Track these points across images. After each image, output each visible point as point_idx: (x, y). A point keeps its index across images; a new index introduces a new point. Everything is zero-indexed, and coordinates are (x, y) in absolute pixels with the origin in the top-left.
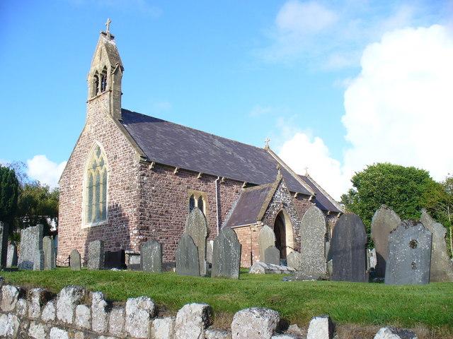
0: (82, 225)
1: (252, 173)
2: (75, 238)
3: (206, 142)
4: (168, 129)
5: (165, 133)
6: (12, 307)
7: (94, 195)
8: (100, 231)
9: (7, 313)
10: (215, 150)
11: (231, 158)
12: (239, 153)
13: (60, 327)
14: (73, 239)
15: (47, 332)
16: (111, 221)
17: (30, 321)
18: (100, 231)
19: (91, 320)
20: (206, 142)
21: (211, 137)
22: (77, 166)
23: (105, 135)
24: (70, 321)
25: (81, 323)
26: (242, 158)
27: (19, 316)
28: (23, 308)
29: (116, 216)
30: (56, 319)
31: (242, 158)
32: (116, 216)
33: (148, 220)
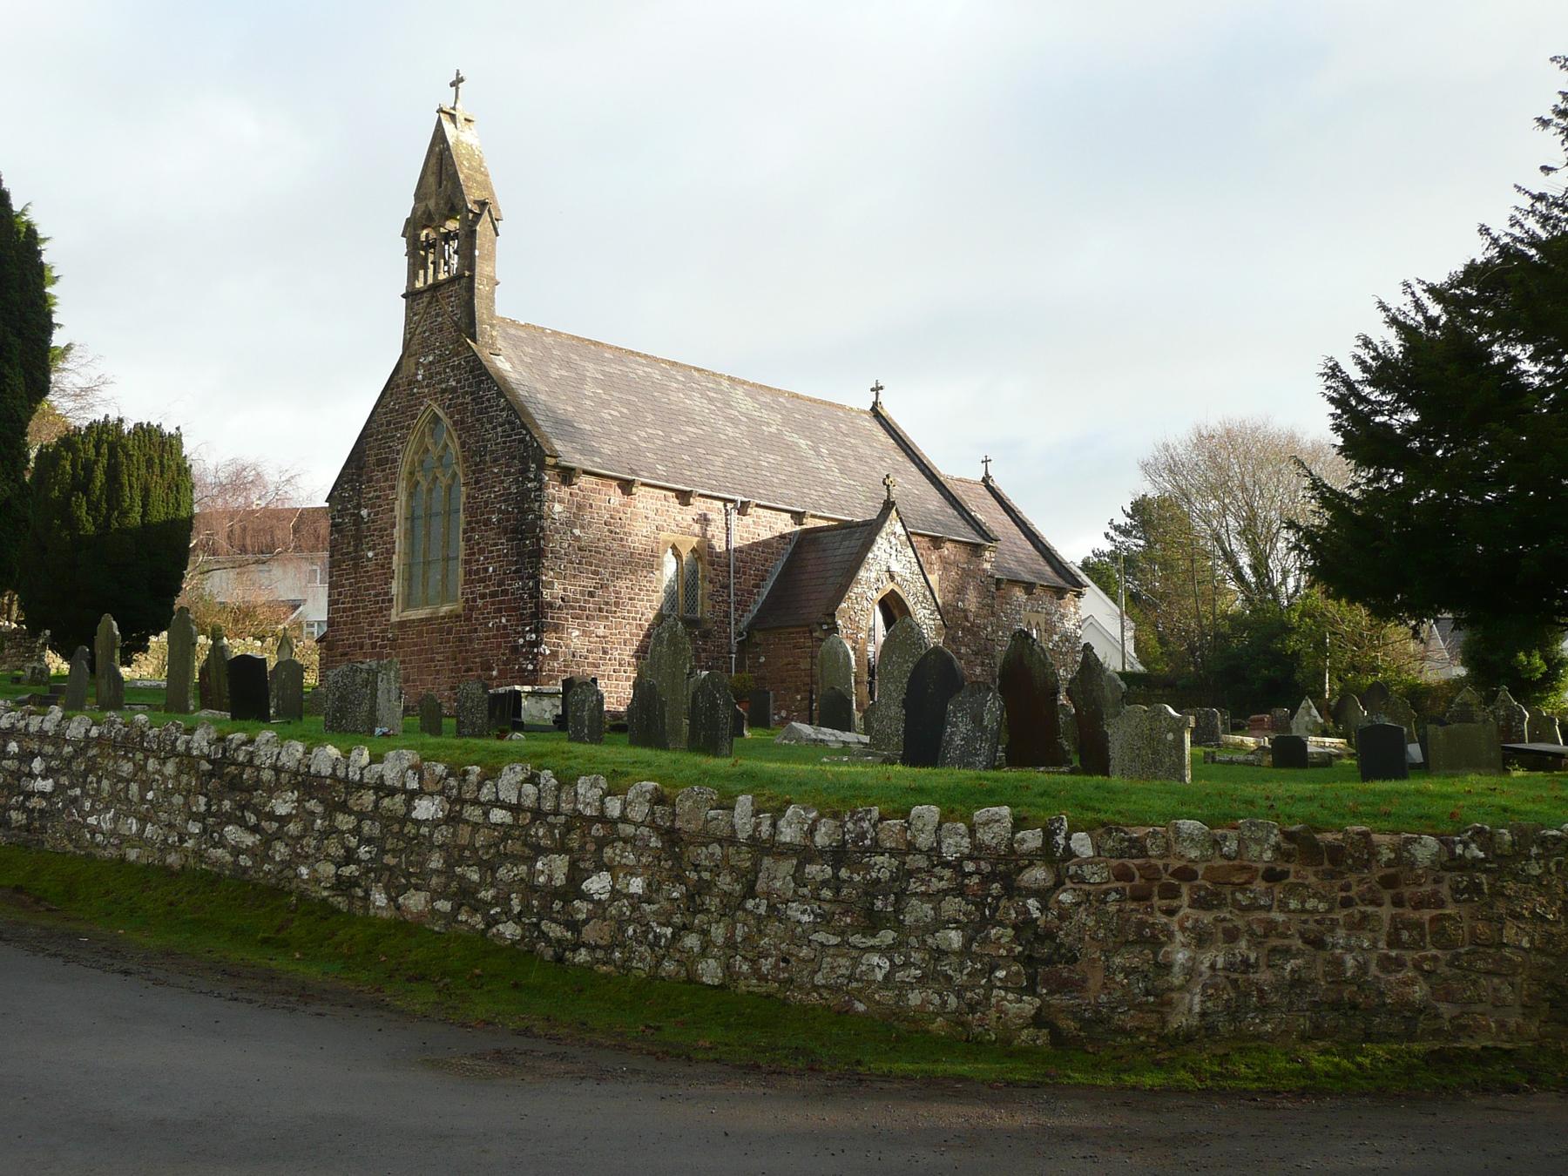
0: (393, 611)
1: (831, 484)
2: (374, 646)
3: (711, 400)
4: (613, 369)
5: (608, 383)
6: (440, 786)
7: (964, 1069)
8: (441, 631)
9: (431, 794)
10: (735, 422)
11: (774, 443)
12: (803, 428)
13: (502, 807)
14: (367, 649)
15: (486, 814)
16: (471, 609)
17: (464, 802)
18: (441, 631)
19: (539, 799)
20: (711, 400)
21: (726, 383)
22: (380, 463)
23: (454, 390)
24: (514, 801)
25: (528, 802)
26: (802, 443)
27: (448, 797)
28: (452, 788)
29: (483, 596)
30: (497, 799)
31: (802, 443)
32: (483, 596)
33: (716, 870)
